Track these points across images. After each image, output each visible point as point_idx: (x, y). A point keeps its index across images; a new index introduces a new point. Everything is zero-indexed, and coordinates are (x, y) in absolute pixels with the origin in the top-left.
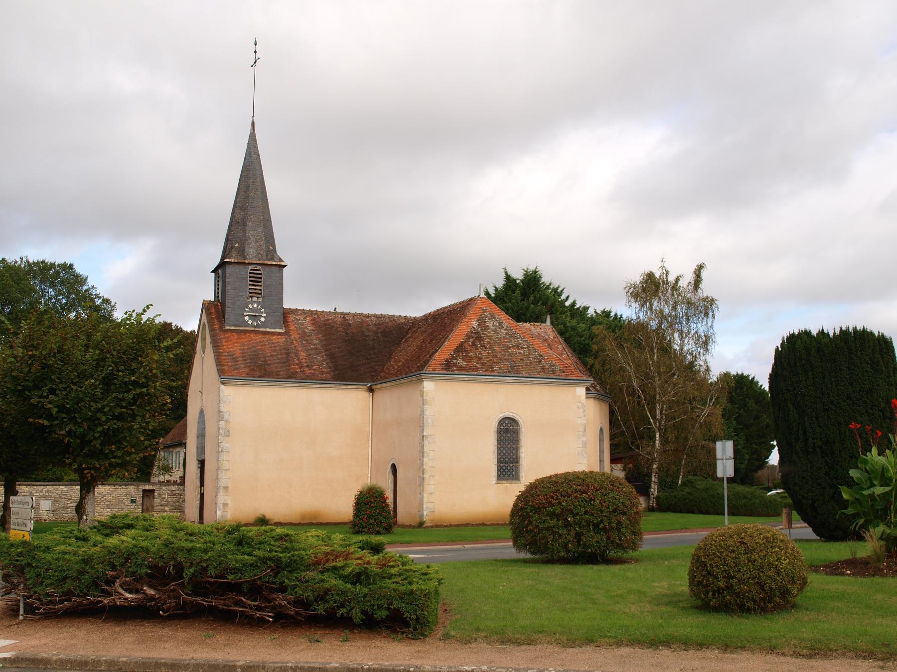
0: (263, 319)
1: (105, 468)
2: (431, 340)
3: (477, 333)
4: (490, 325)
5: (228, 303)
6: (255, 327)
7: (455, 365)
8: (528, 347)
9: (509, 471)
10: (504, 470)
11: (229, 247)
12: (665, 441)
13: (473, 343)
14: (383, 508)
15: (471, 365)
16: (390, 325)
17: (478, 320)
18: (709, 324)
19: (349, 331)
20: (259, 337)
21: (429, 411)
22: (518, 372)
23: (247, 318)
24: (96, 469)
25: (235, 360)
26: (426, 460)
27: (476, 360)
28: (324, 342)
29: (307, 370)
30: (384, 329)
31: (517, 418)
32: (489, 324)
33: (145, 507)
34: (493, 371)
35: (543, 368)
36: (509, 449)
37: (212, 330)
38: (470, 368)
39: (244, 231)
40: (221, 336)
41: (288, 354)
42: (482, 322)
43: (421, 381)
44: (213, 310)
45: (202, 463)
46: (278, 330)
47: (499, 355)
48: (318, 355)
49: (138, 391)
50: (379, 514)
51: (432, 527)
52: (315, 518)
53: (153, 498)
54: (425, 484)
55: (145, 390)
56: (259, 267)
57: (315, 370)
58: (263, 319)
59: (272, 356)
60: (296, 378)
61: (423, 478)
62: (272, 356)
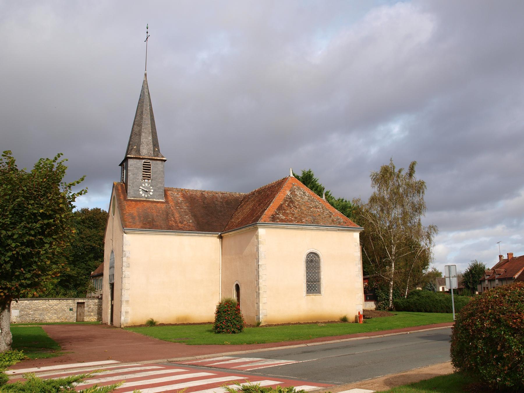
0: (151, 193)
1: (16, 288)
2: (259, 205)
3: (290, 198)
4: (298, 194)
5: (129, 183)
6: (146, 198)
7: (278, 218)
8: (322, 207)
9: (314, 287)
11: (130, 149)
12: (397, 268)
13: (288, 205)
14: (236, 314)
15: (288, 218)
16: (230, 198)
17: (290, 191)
18: (421, 196)
19: (205, 201)
20: (148, 205)
21: (262, 248)
22: (318, 223)
23: (141, 192)
24: (9, 289)
25: (133, 218)
26: (260, 281)
27: (291, 215)
28: (190, 208)
29: (180, 225)
30: (227, 201)
31: (318, 253)
32: (297, 193)
33: (78, 313)
34: (302, 222)
35: (333, 221)
36: (313, 273)
37: (119, 200)
38: (288, 220)
39: (140, 138)
40: (125, 203)
41: (167, 215)
42: (293, 192)
43: (256, 229)
44: (120, 188)
45: (112, 285)
46: (161, 200)
47: (305, 212)
48: (186, 215)
49: (46, 222)
50: (234, 318)
51: (266, 326)
52: (186, 319)
53: (84, 307)
54: (260, 297)
55: (52, 221)
56: (149, 161)
57: (185, 225)
59: (157, 216)
60: (173, 229)
61: (259, 293)
62: (157, 216)
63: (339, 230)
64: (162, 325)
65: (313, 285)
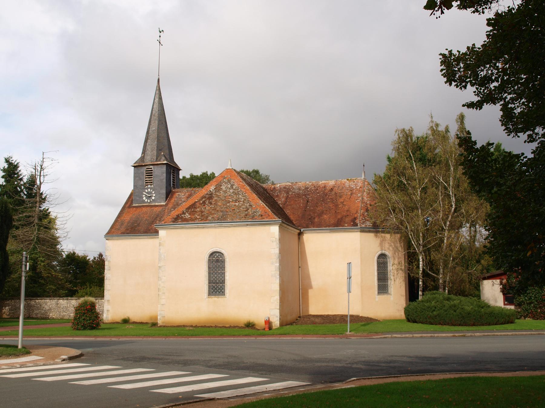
0: (153, 198)
9: (219, 289)
10: (216, 289)
31: (223, 251)
46: (162, 204)
58: (153, 198)
63: (247, 225)
64: (134, 323)
65: (216, 286)
